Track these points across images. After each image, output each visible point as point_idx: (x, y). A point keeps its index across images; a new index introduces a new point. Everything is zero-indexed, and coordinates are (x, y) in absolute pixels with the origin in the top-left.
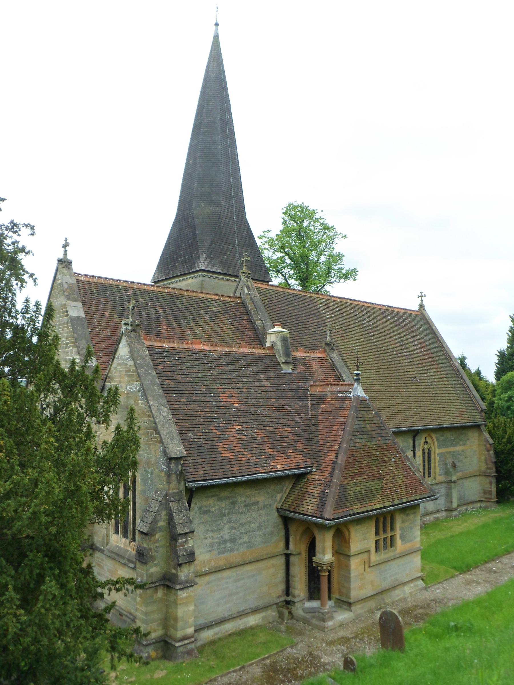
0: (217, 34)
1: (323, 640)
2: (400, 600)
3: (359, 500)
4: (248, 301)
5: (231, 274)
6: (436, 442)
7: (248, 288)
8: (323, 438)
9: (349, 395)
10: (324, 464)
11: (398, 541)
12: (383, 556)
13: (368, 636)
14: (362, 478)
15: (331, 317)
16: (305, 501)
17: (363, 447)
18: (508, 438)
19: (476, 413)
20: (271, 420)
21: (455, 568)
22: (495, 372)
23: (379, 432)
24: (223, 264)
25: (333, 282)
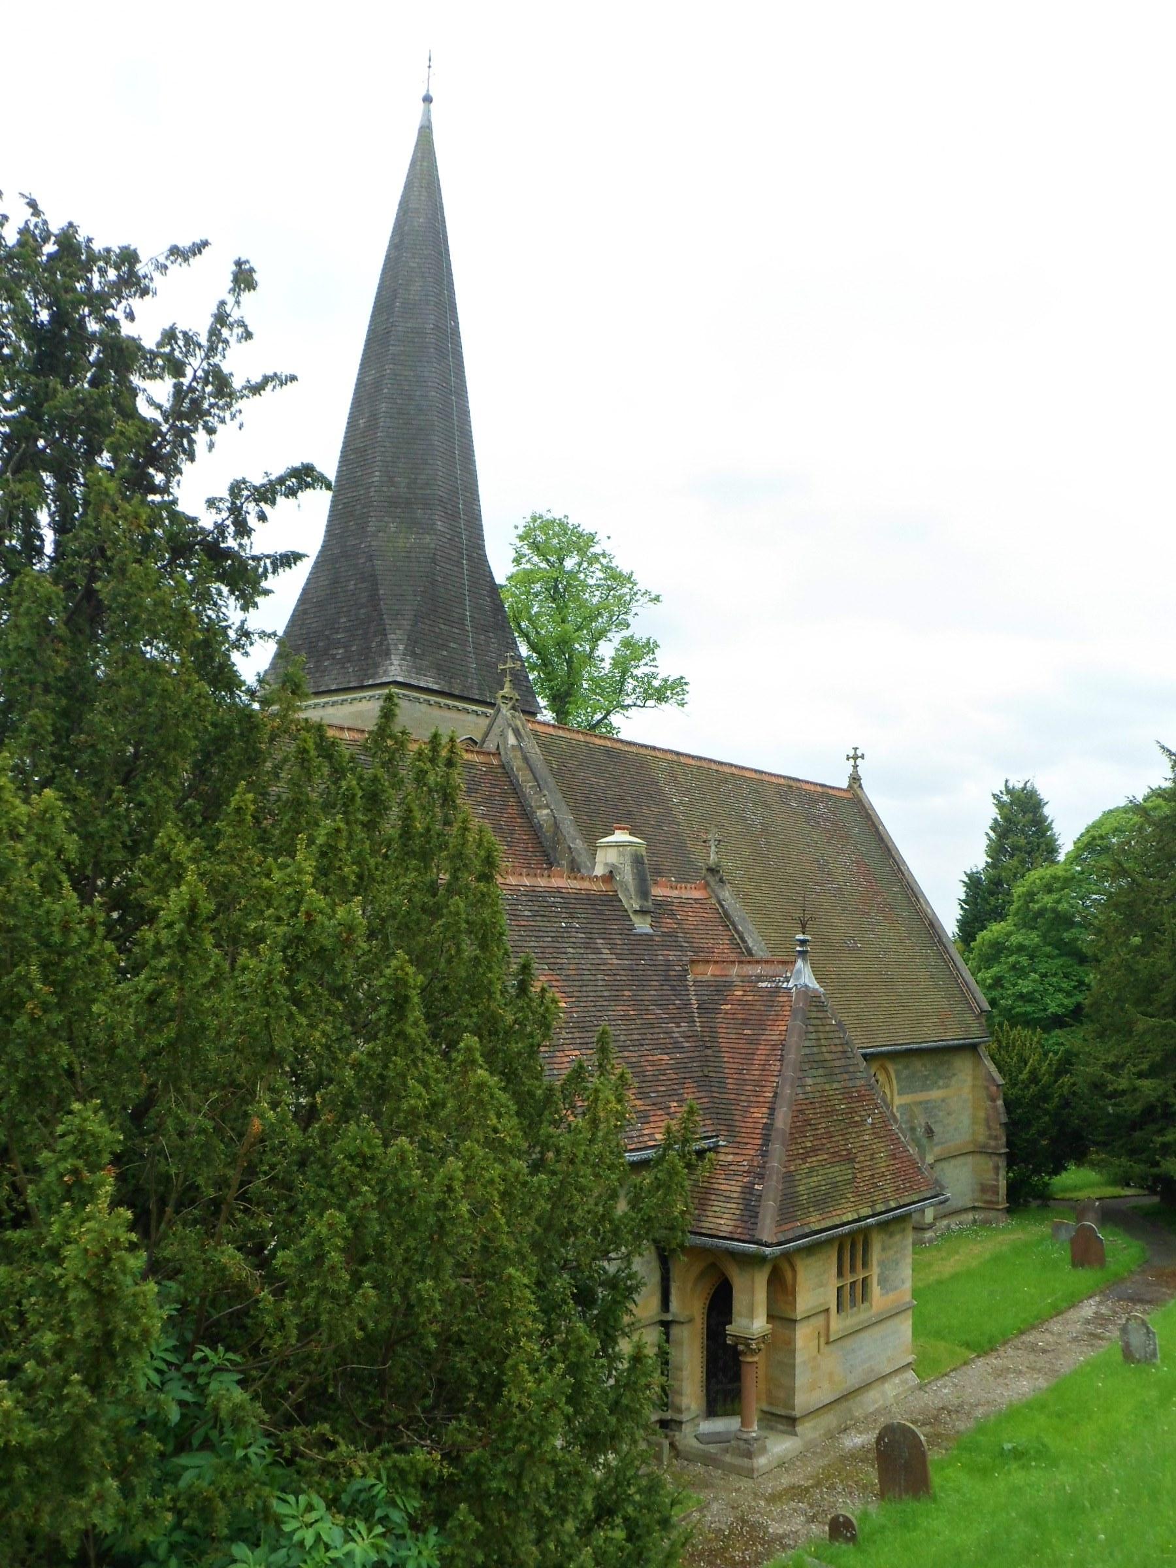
0: (429, 121)
1: (755, 1494)
2: (877, 1412)
3: (816, 1204)
4: (517, 764)
5: (457, 692)
6: (895, 1082)
7: (517, 733)
8: (735, 1076)
9: (785, 985)
10: (744, 1130)
11: (876, 1290)
12: (852, 1319)
13: (842, 1481)
14: (820, 1158)
15: (681, 803)
16: (709, 1208)
17: (817, 1094)
18: (1030, 1072)
19: (969, 1018)
20: (630, 1037)
21: (967, 1345)
22: (958, 921)
23: (843, 1062)
24: (441, 670)
25: (629, 706)
